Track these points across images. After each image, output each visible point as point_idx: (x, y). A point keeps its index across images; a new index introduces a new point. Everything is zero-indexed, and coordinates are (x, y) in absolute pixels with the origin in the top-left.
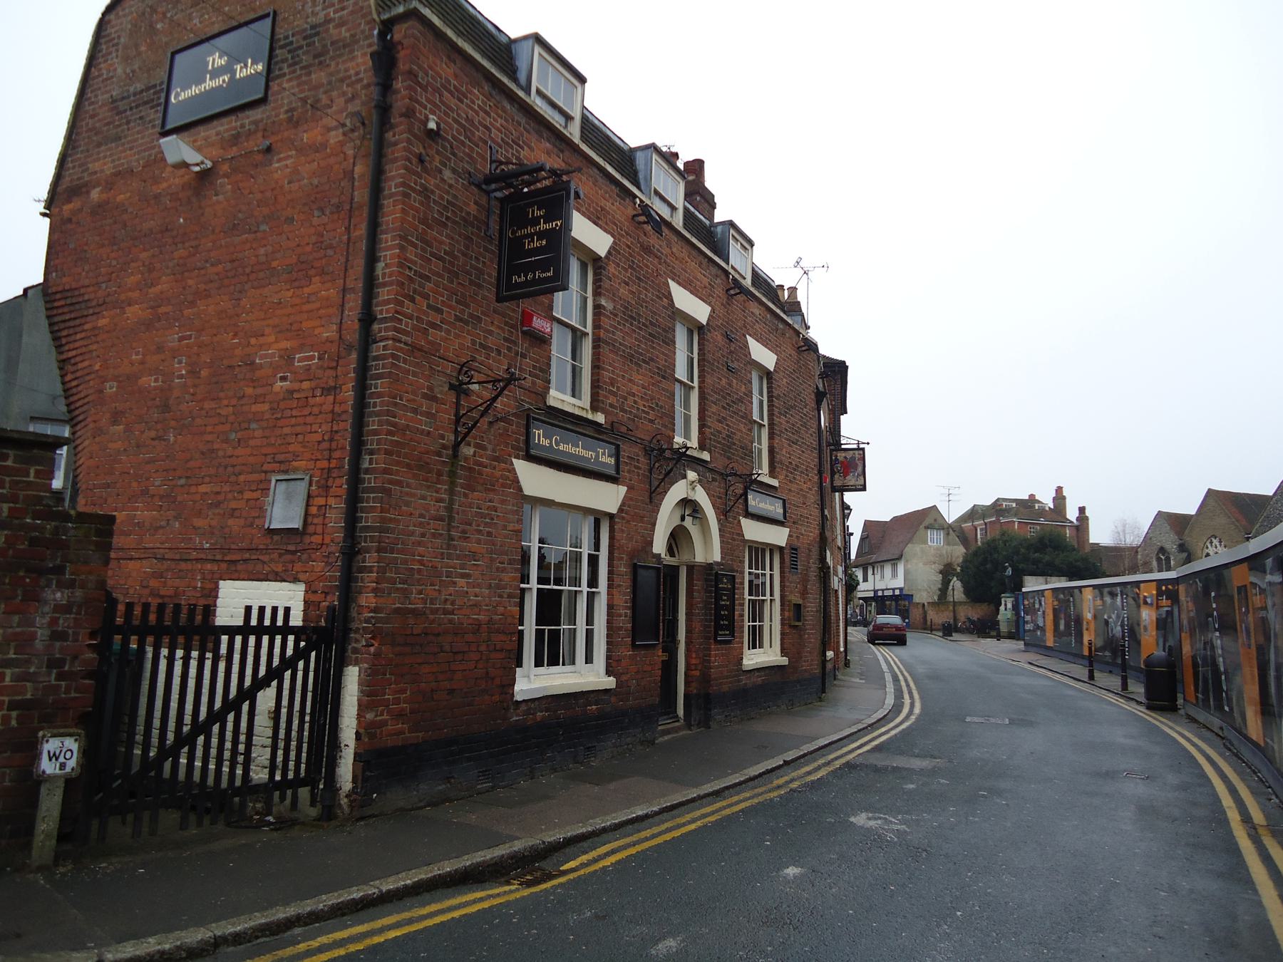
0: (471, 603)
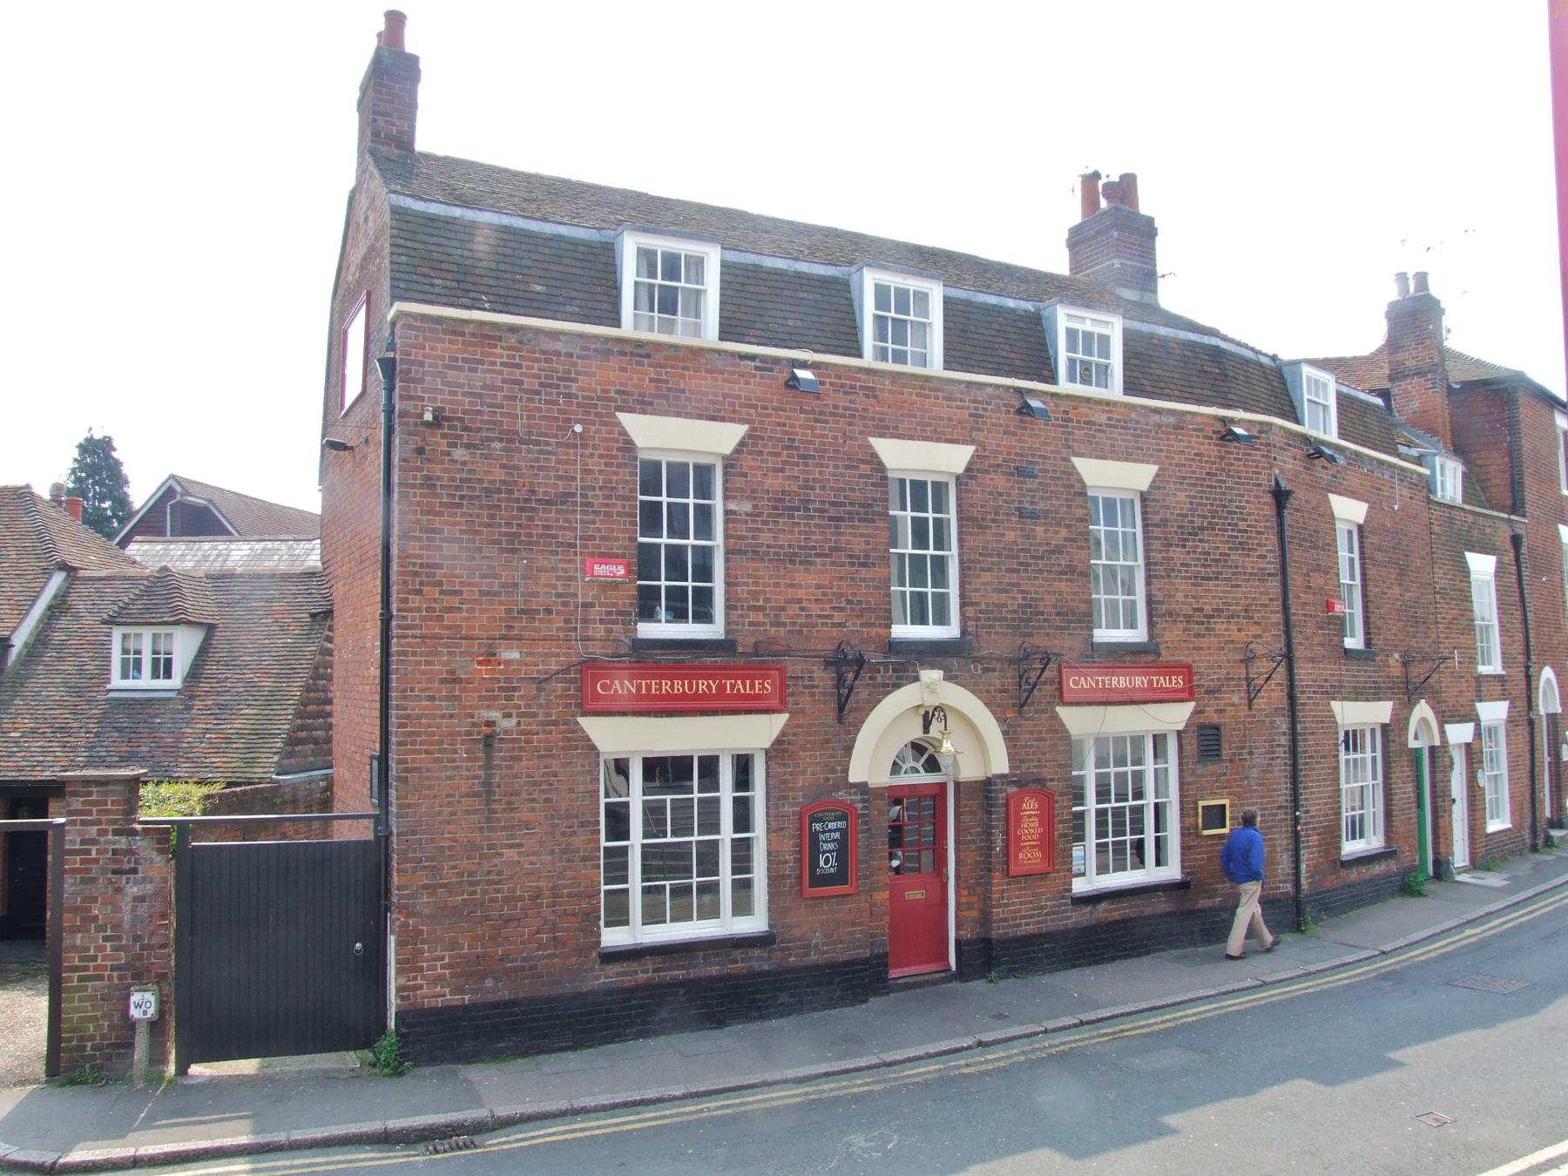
0: (525, 872)
